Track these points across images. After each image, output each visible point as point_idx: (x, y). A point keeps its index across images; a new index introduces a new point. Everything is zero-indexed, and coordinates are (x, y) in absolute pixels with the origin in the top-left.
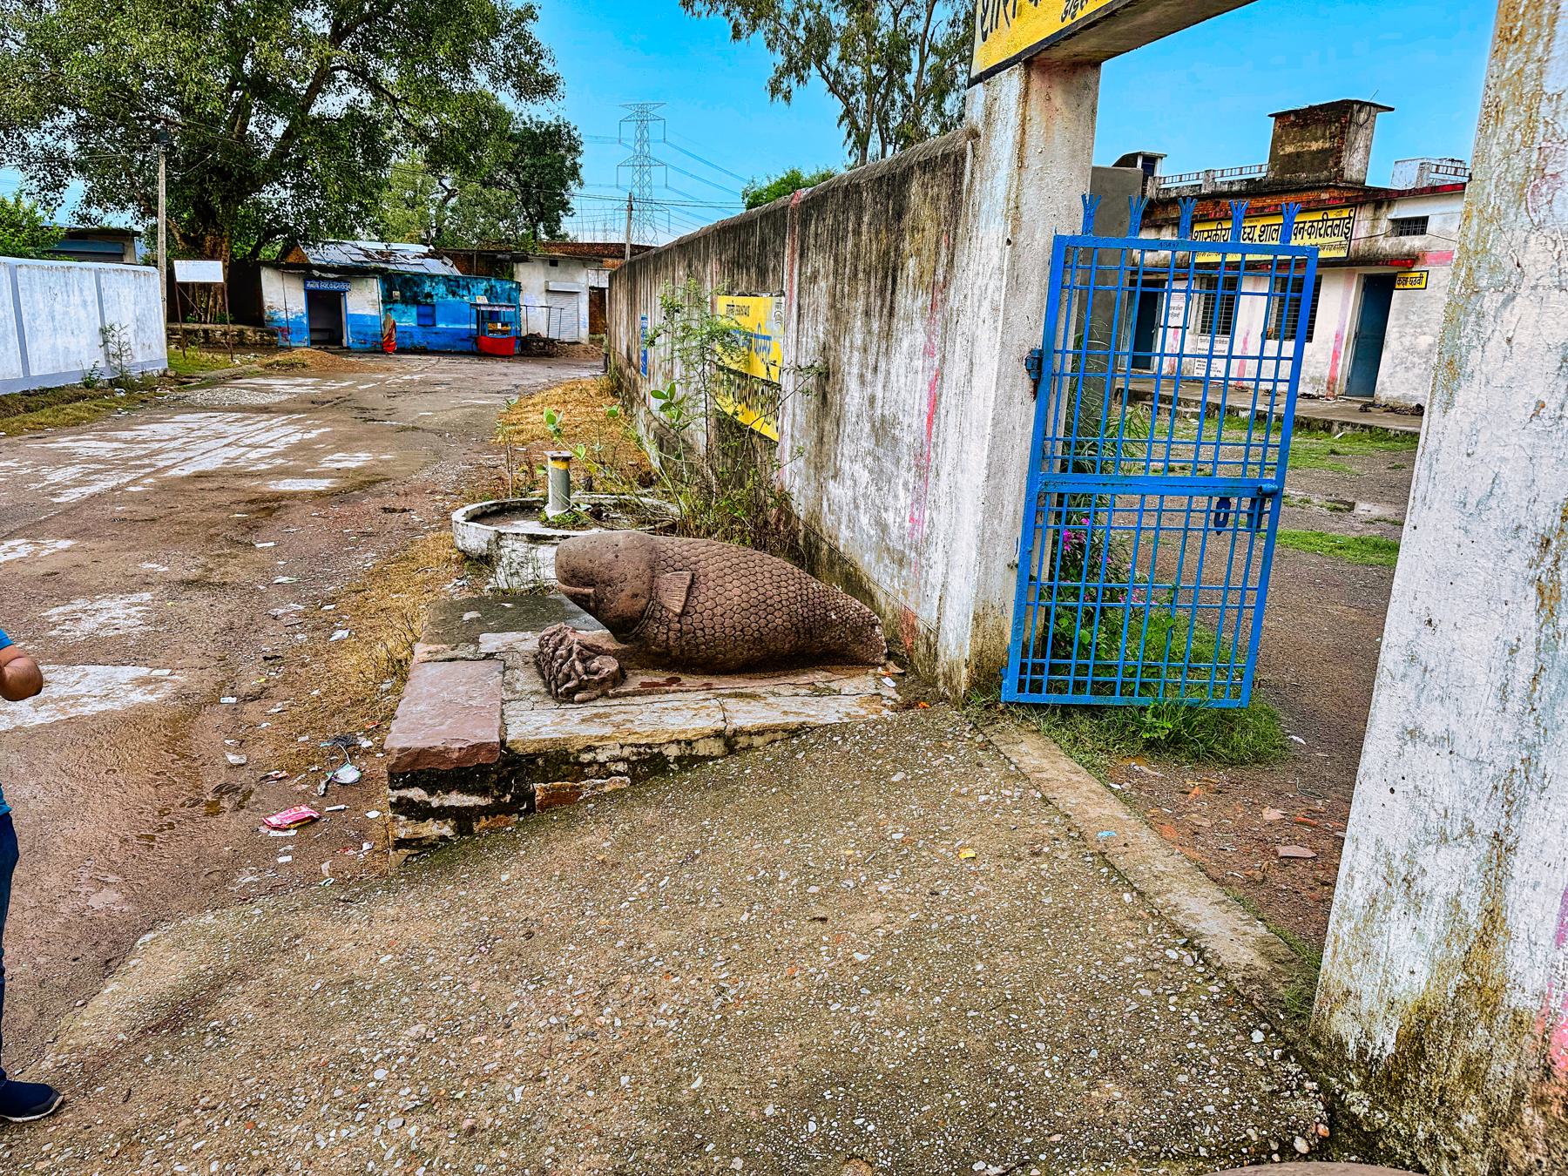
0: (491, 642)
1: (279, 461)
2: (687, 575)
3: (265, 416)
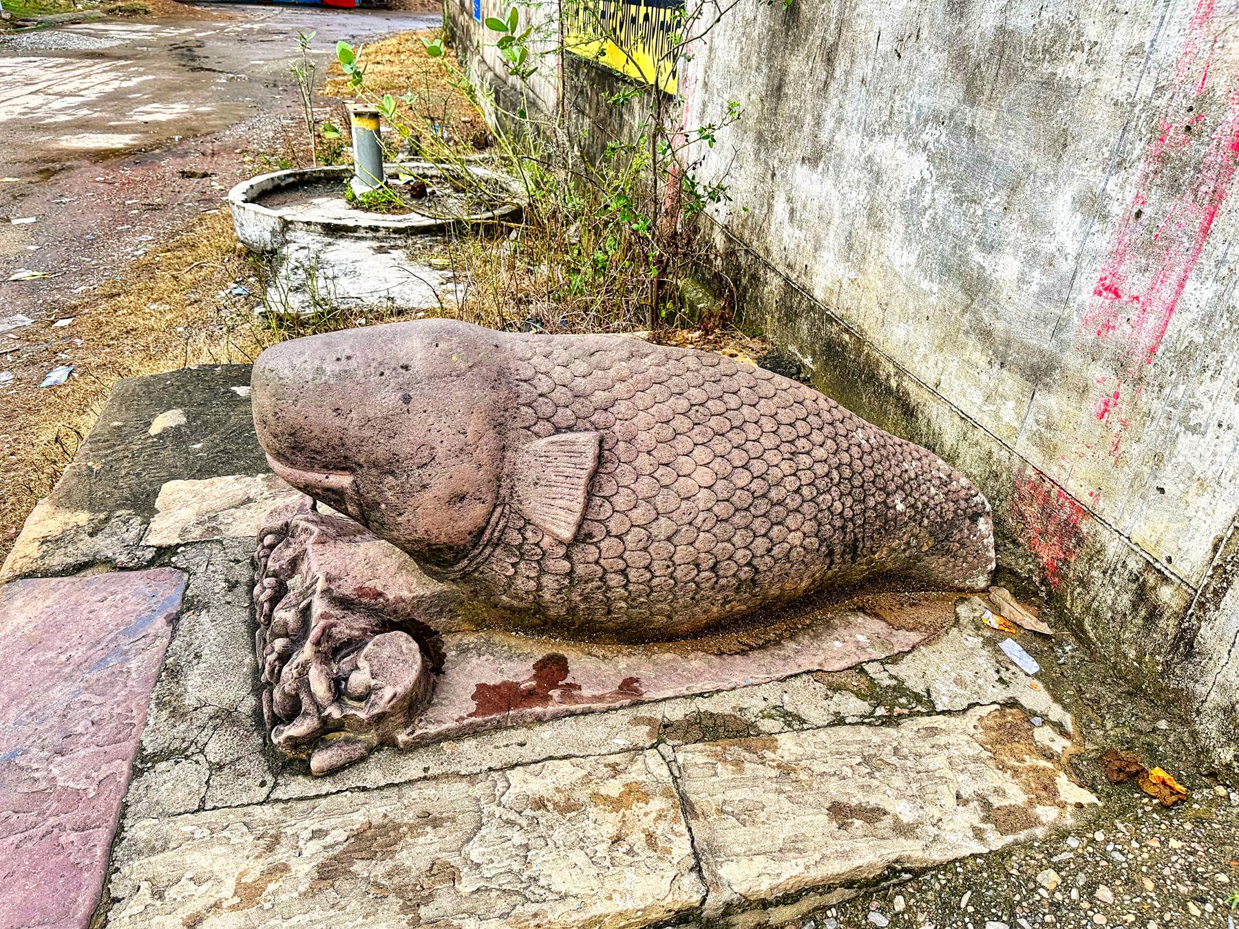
1: (85, 112)
2: (586, 441)
3: (90, 62)
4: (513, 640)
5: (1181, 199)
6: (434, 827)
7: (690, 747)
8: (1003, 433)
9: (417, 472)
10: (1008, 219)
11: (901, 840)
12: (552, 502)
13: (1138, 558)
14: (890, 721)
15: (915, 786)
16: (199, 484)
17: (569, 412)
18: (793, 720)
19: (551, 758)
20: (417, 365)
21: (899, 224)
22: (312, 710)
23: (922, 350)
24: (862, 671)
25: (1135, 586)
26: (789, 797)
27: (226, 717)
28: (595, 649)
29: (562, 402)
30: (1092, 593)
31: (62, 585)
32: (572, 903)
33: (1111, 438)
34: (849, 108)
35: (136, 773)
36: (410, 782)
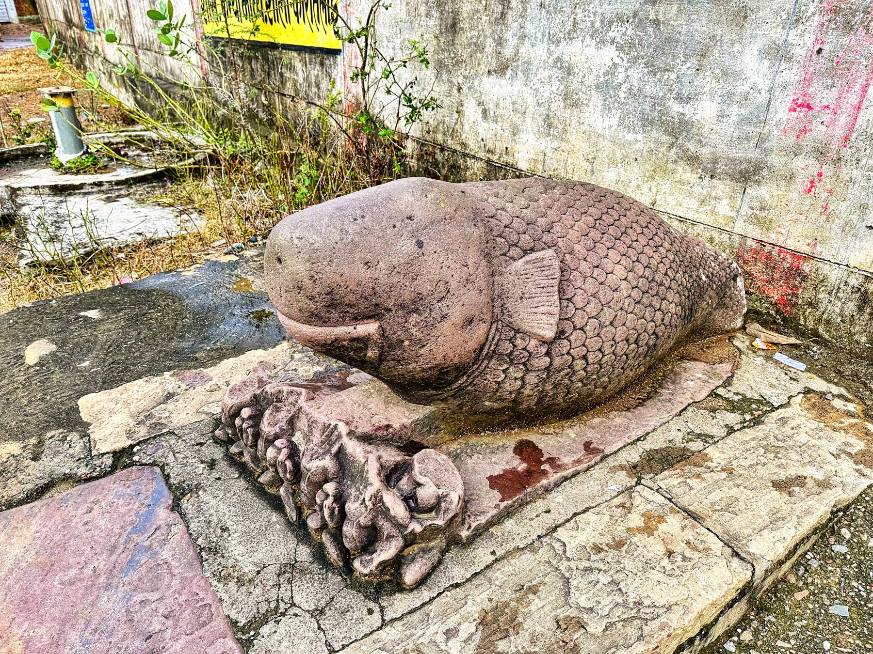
0: (109, 416)
4: (485, 439)
5: (855, 34)
6: (535, 593)
7: (660, 476)
8: (721, 223)
9: (437, 305)
10: (701, 76)
11: (828, 490)
12: (536, 310)
13: (857, 276)
14: (757, 421)
15: (806, 455)
16: (114, 393)
19: (575, 514)
20: (418, 214)
21: (596, 99)
22: (394, 531)
23: (635, 183)
24: (717, 395)
25: (858, 295)
26: (745, 487)
27: (290, 570)
28: (545, 429)
29: (521, 230)
30: (821, 309)
31: (36, 510)
32: (678, 611)
33: (820, 203)
34: (528, 25)
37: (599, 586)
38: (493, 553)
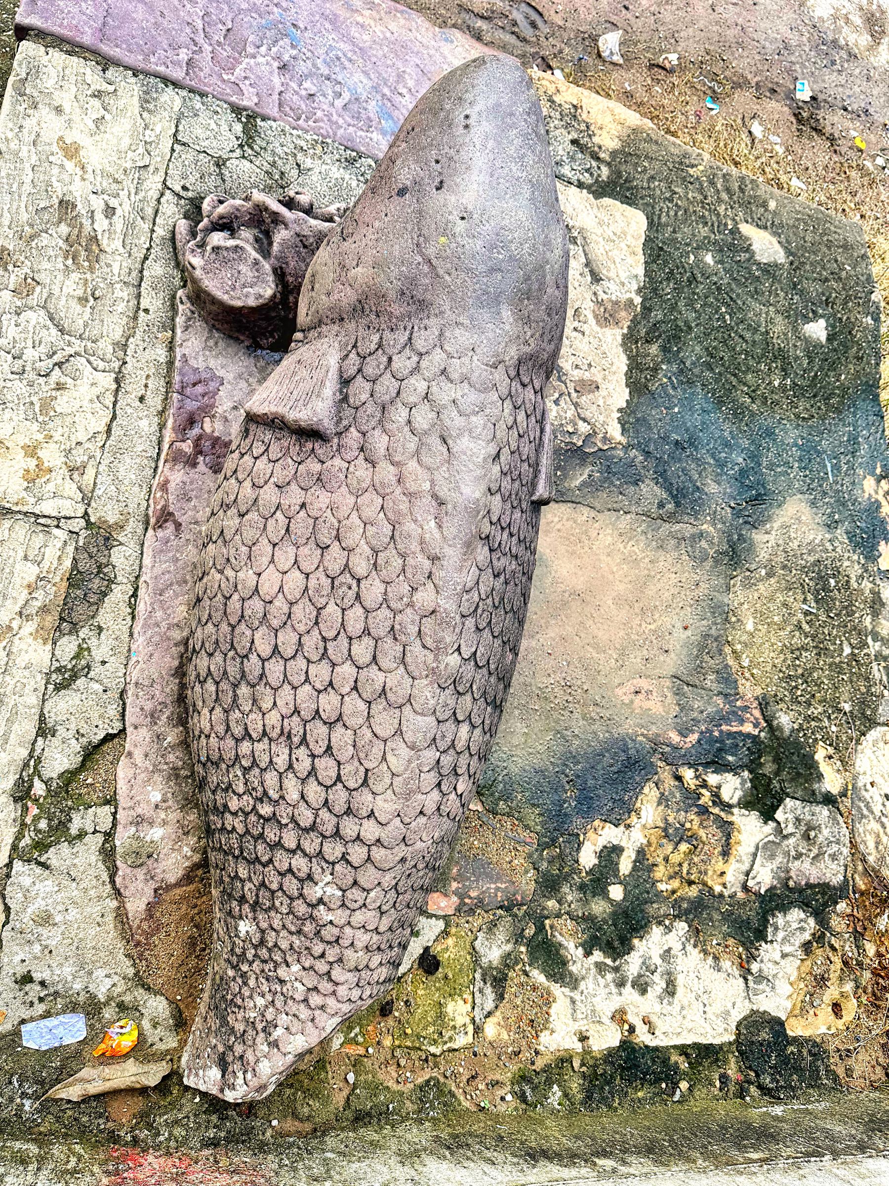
7: (70, 549)
17: (364, 397)
18: (65, 678)
19: (114, 417)
20: (441, 196)
35: (237, 110)
36: (139, 296)
37: (30, 343)
38: (146, 311)
